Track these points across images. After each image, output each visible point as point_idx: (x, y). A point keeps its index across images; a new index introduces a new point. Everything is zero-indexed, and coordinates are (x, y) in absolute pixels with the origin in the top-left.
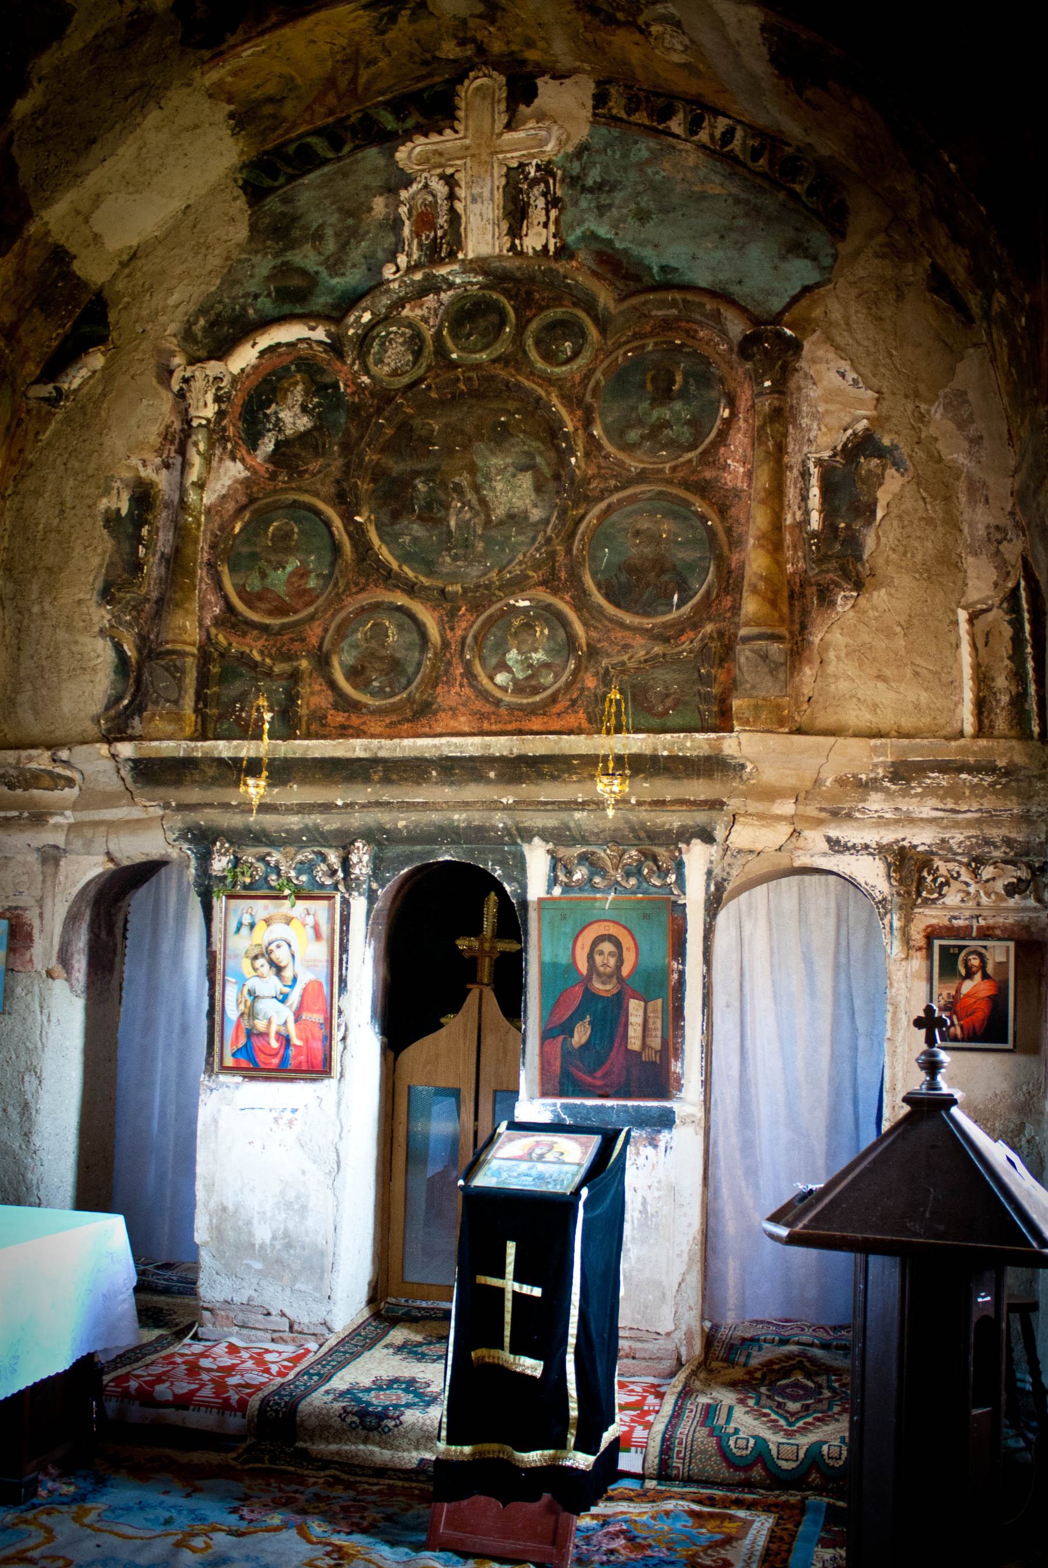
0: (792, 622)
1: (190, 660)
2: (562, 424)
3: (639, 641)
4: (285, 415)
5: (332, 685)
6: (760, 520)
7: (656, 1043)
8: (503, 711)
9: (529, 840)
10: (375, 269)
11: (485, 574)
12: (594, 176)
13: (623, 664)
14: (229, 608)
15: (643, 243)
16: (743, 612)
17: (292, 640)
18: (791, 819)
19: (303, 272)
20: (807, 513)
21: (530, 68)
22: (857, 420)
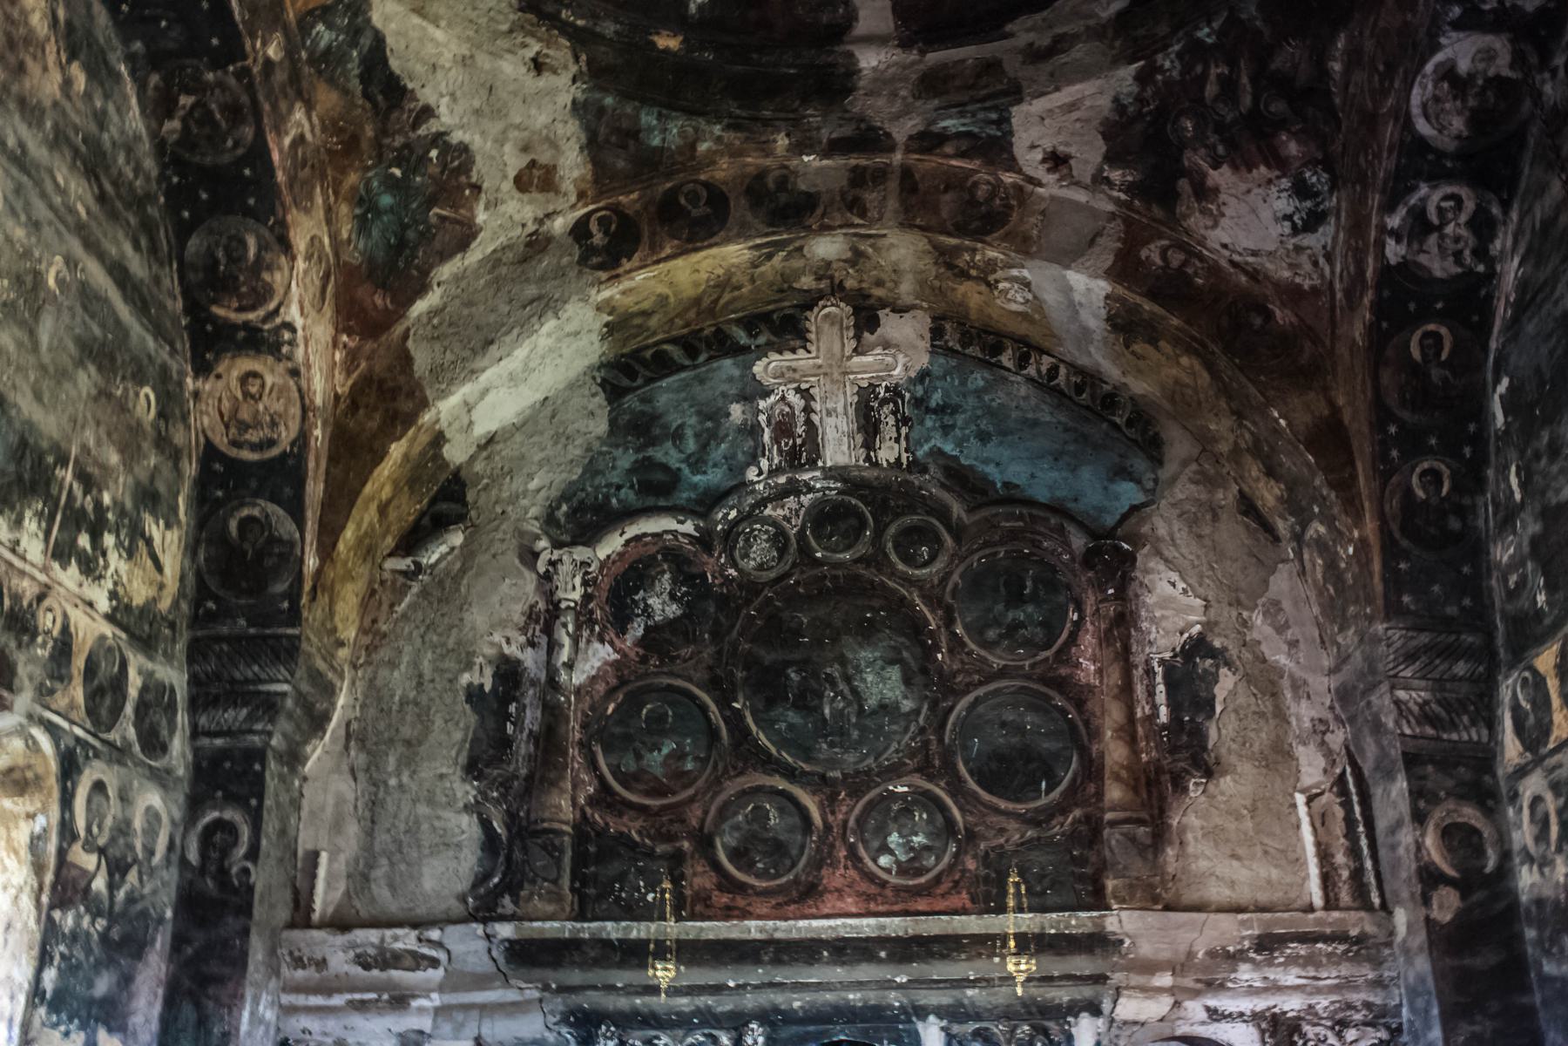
0: (1152, 807)
1: (566, 838)
2: (928, 624)
3: (1012, 825)
4: (654, 602)
5: (716, 866)
6: (1114, 714)
8: (888, 892)
10: (738, 470)
11: (862, 761)
12: (936, 398)
13: (1002, 846)
15: (986, 461)
17: (671, 821)
18: (1171, 991)
19: (665, 468)
20: (1155, 707)
21: (872, 301)
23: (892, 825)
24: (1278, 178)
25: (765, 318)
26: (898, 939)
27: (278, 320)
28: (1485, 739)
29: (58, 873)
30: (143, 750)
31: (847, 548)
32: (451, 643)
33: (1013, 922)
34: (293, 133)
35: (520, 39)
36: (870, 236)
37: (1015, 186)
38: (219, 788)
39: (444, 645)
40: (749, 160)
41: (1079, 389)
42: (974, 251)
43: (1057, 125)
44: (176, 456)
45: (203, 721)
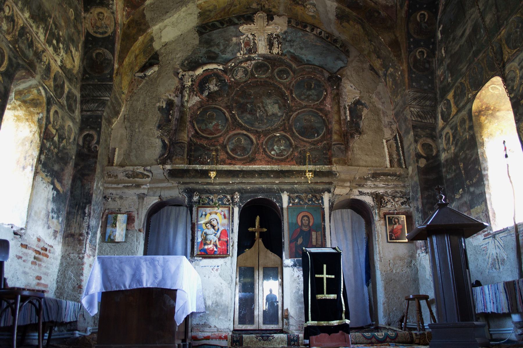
2: (285, 93)
3: (307, 145)
4: (211, 86)
5: (227, 153)
6: (336, 117)
8: (274, 160)
9: (283, 192)
12: (289, 38)
14: (196, 132)
15: (302, 54)
16: (333, 139)
18: (349, 187)
19: (214, 53)
20: (346, 117)
21: (272, 13)
25: (243, 16)
31: (265, 74)
32: (154, 95)
38: (88, 125)
39: (152, 96)
41: (327, 38)
44: (79, 32)
45: (84, 107)
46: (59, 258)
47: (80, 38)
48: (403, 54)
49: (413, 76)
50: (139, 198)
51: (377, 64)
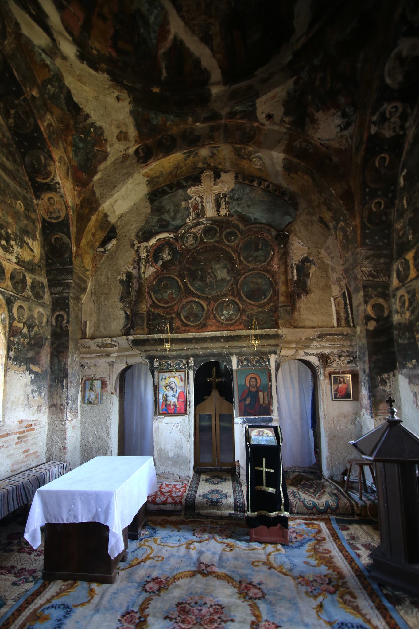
3: (255, 308)
5: (181, 320)
6: (283, 278)
7: (266, 402)
8: (223, 325)
12: (236, 196)
14: (154, 302)
15: (249, 213)
18: (295, 348)
19: (165, 220)
20: (293, 276)
21: (219, 170)
22: (304, 254)
23: (224, 309)
24: (337, 112)
25: (190, 177)
26: (226, 337)
27: (55, 181)
28: (387, 280)
29: (10, 328)
30: (35, 298)
31: (213, 238)
32: (115, 269)
33: (254, 332)
34: (47, 122)
35: (112, 90)
36: (216, 147)
37: (258, 128)
40: (181, 126)
41: (275, 191)
42: (245, 149)
43: (269, 105)
44: (33, 221)
45: (52, 290)
46: (47, 425)
47: (36, 227)
48: (356, 208)
49: (367, 231)
50: (109, 365)
51: (328, 216)
